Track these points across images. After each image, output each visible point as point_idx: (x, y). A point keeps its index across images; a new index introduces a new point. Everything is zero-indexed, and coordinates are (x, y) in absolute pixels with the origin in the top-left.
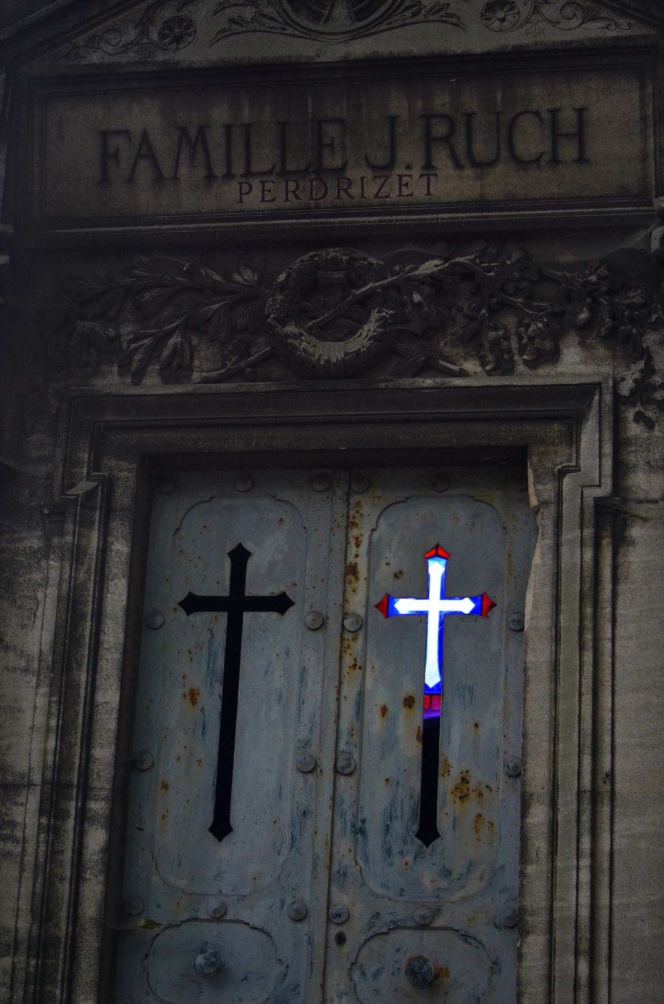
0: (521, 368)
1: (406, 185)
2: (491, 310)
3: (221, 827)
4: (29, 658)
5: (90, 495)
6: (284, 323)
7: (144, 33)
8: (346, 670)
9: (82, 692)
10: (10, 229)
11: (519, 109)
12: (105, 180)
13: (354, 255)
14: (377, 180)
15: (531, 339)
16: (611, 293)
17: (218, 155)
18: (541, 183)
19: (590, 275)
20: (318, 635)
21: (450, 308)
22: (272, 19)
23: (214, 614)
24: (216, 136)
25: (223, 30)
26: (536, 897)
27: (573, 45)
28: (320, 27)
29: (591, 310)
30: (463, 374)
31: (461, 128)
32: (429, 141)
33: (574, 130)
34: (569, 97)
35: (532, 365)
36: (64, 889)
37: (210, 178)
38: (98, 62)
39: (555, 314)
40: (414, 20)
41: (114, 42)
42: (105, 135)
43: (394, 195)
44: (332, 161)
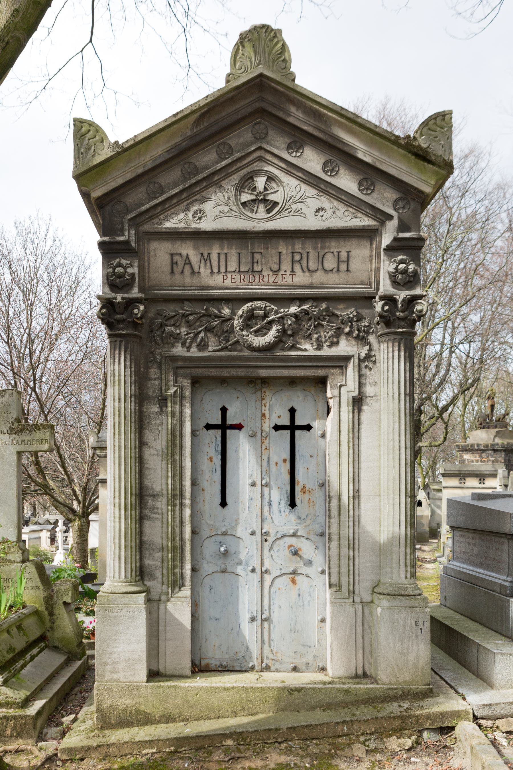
0: (325, 348)
2: (315, 326)
3: (224, 503)
4: (158, 451)
5: (175, 392)
6: (242, 330)
7: (186, 215)
8: (263, 450)
9: (178, 463)
10: (143, 295)
11: (326, 251)
12: (172, 272)
15: (329, 338)
16: (357, 321)
17: (215, 264)
20: (253, 439)
23: (216, 430)
24: (214, 257)
25: (217, 216)
26: (334, 529)
28: (253, 215)
30: (306, 350)
31: (305, 258)
32: (293, 261)
34: (343, 248)
35: (330, 346)
36: (177, 530)
37: (212, 272)
39: (338, 328)
42: (172, 255)
43: (280, 282)
44: (257, 268)
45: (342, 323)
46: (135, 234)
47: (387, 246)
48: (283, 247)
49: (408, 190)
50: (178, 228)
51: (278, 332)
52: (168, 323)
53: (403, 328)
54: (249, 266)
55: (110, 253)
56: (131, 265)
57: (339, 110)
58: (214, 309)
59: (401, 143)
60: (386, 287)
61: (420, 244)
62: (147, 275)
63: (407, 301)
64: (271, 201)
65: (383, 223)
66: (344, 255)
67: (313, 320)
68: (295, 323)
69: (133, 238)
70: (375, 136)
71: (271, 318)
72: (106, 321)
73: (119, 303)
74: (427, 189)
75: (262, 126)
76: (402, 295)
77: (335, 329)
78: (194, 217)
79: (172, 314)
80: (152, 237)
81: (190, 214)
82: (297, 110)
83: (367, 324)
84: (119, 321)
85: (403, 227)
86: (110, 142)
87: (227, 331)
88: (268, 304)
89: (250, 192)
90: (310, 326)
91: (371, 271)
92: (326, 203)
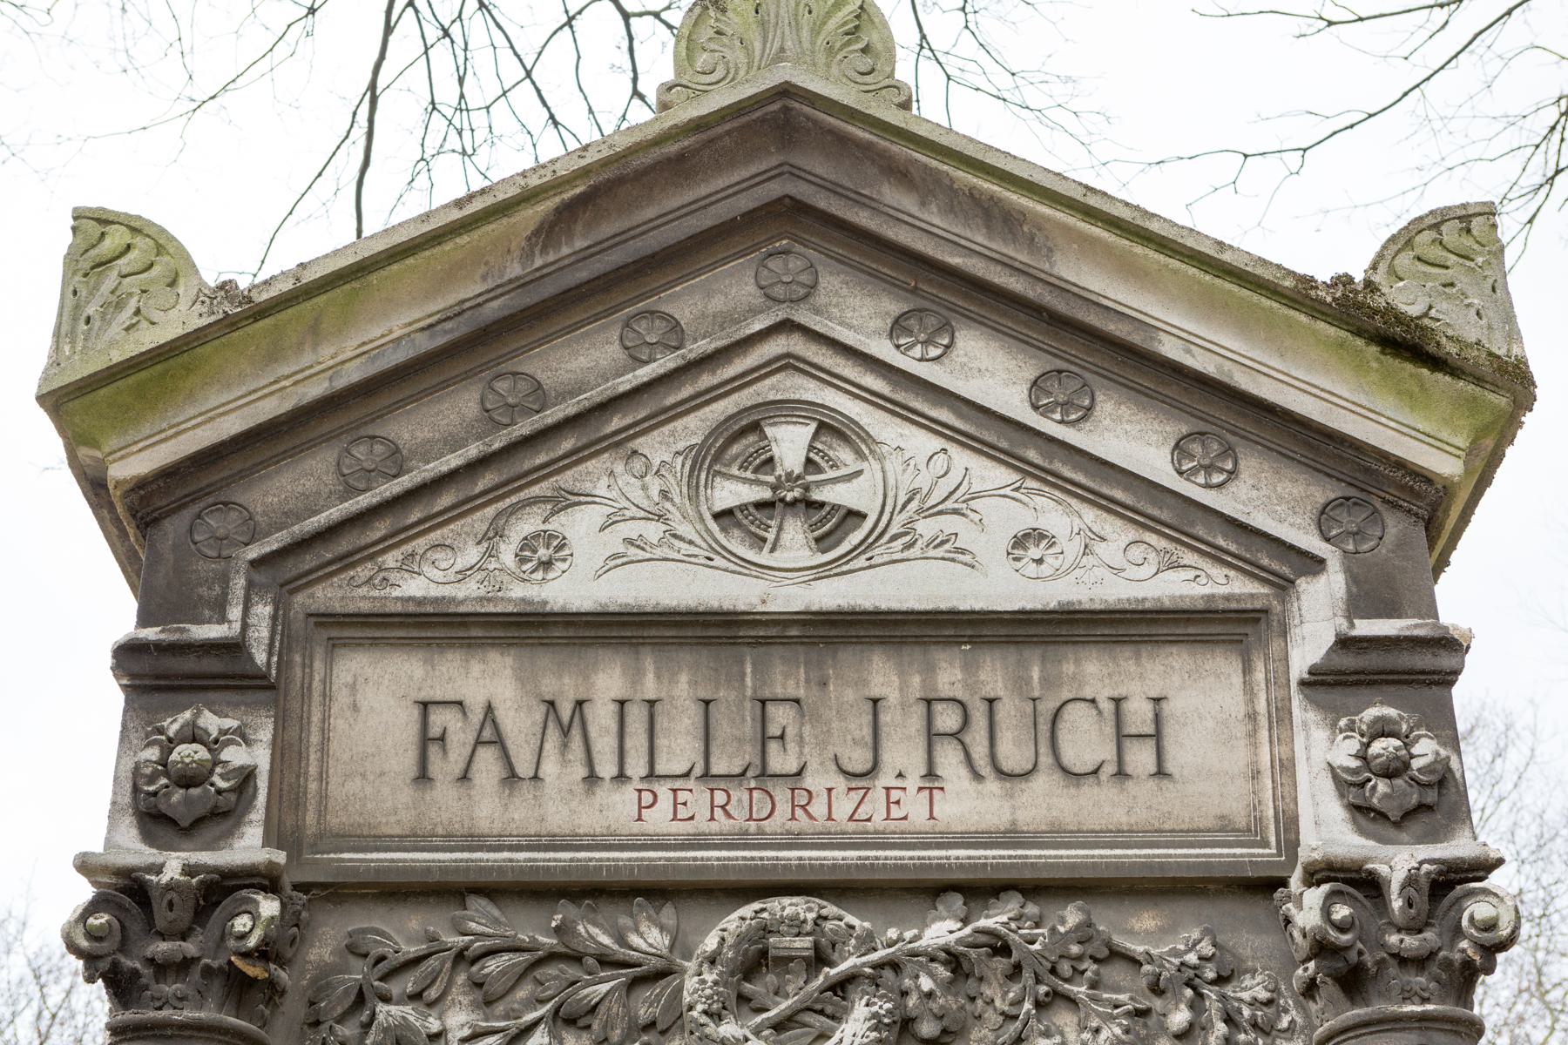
1: (898, 802)
2: (1038, 1005)
6: (717, 1017)
7: (491, 554)
10: (280, 857)
12: (423, 776)
13: (824, 912)
14: (852, 793)
16: (1221, 980)
17: (605, 746)
18: (1102, 806)
19: (1186, 952)
21: (973, 999)
22: (691, 542)
24: (602, 717)
25: (615, 556)
27: (1148, 605)
28: (764, 558)
29: (1191, 1007)
32: (932, 736)
33: (1150, 730)
37: (592, 778)
38: (419, 594)
40: (906, 554)
41: (444, 565)
42: (425, 706)
44: (781, 760)
45: (1156, 989)
46: (274, 618)
47: (1313, 671)
48: (884, 675)
49: (1367, 470)
50: (452, 600)
51: (875, 1028)
52: (395, 988)
53: (1425, 1000)
54: (749, 754)
55: (158, 689)
56: (243, 736)
57: (1077, 194)
58: (594, 931)
59: (1323, 302)
60: (1328, 830)
61: (1445, 661)
62: (313, 786)
63: (1424, 884)
64: (835, 508)
65: (1284, 586)
66: (1139, 714)
67: (1027, 975)
68: (949, 986)
69: (261, 632)
70: (1218, 281)
71: (844, 966)
72: (104, 965)
73: (171, 887)
74: (1446, 466)
75: (795, 263)
76: (1400, 861)
77: (1128, 1014)
78: (523, 561)
79: (413, 950)
80: (346, 633)
81: (507, 553)
82: (923, 204)
83: (1263, 995)
84: (162, 968)
85: (1361, 601)
86: (202, 283)
87: (651, 1025)
88: (831, 909)
89: (749, 475)
90: (1019, 1002)
91: (1256, 775)
92: (1056, 516)
